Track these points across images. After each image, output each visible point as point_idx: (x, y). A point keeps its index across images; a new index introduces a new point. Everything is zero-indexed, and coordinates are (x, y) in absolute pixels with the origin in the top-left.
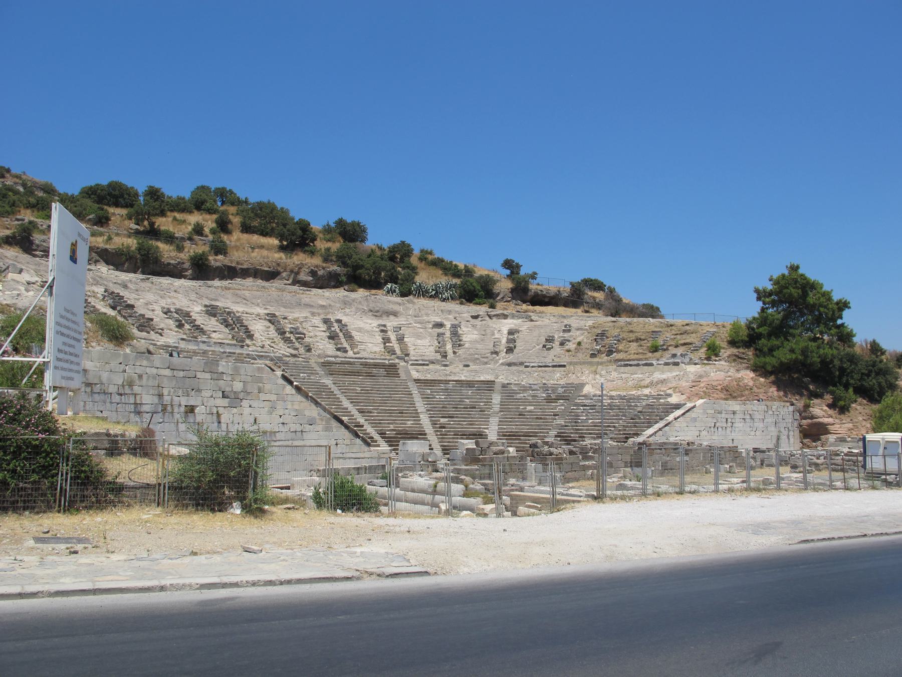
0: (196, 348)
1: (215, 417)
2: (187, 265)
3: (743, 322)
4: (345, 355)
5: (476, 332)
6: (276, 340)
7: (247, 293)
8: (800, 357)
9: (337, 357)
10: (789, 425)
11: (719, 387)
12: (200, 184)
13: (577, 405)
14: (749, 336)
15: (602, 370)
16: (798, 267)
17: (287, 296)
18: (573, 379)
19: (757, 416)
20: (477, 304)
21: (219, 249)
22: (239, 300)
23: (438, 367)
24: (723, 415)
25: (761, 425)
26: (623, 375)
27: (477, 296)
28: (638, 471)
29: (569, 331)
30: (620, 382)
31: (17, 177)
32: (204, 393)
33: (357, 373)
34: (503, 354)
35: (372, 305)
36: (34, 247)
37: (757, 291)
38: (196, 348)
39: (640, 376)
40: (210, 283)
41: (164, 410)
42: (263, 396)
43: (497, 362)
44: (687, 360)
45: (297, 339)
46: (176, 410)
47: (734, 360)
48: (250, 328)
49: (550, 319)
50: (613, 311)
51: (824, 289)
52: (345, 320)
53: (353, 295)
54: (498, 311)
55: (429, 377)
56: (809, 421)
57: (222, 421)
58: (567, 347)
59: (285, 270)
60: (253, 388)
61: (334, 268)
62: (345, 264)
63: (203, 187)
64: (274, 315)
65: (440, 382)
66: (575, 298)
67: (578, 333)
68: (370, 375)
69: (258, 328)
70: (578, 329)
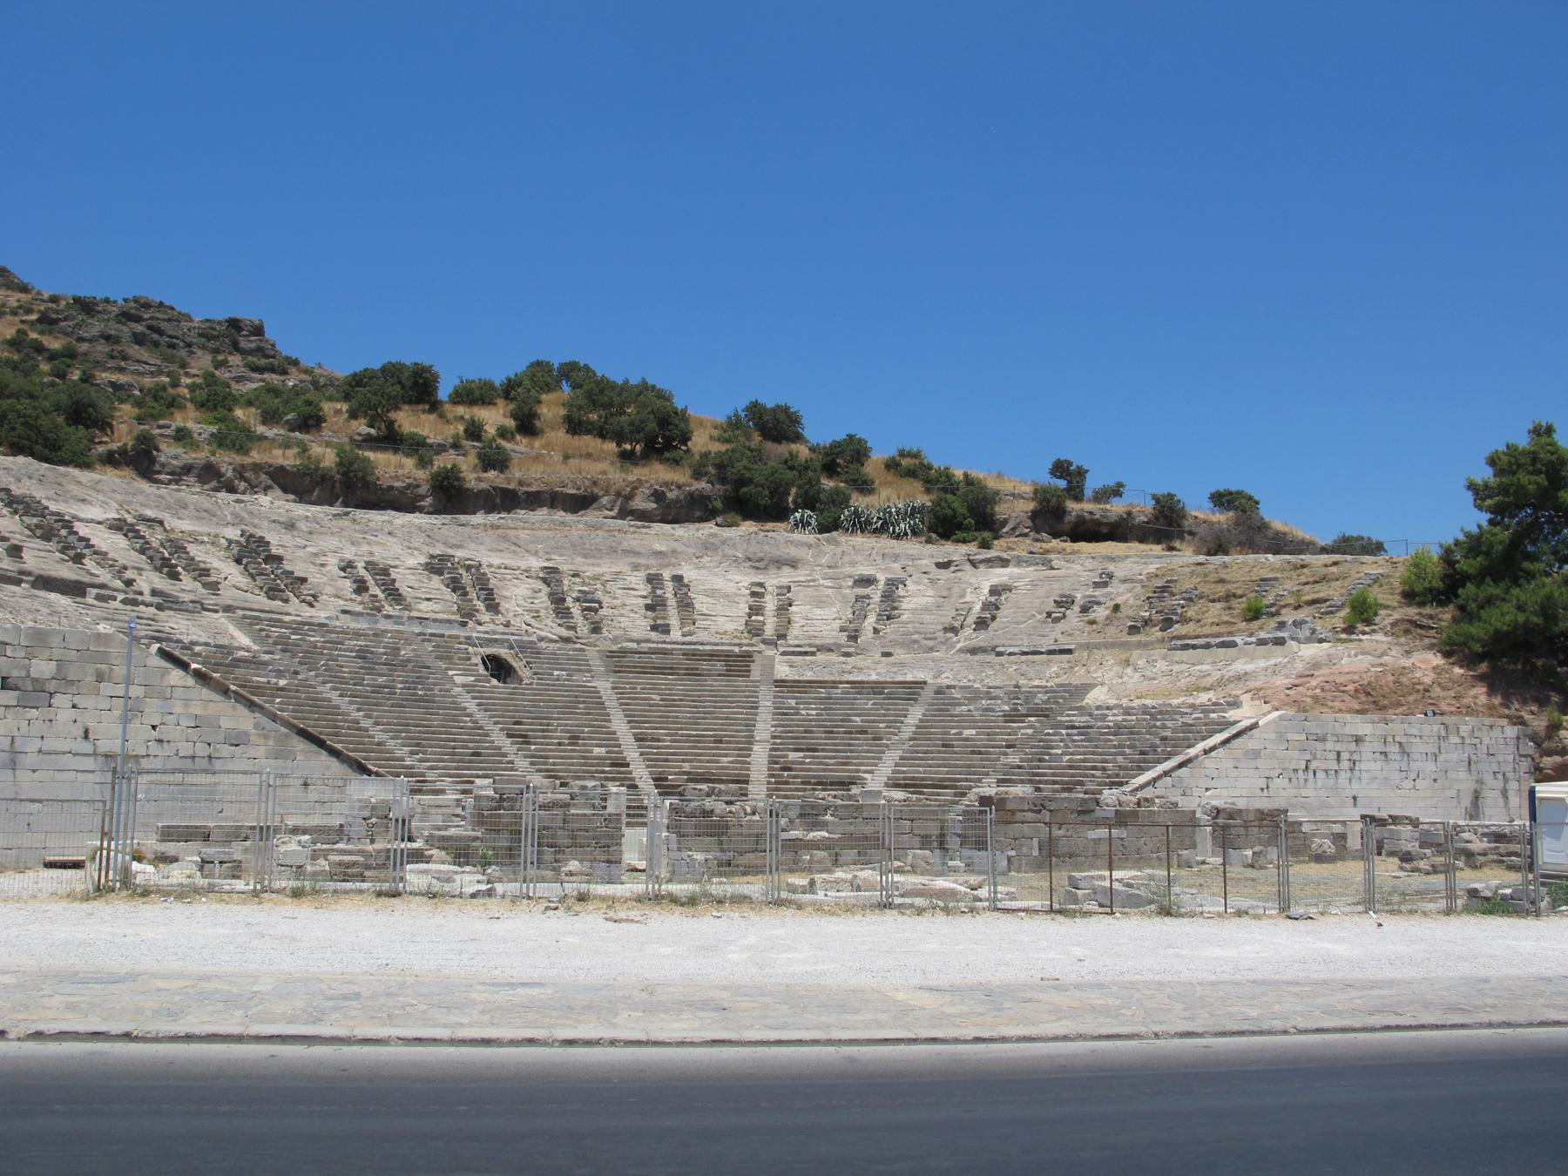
2: (423, 490)
3: (1435, 554)
5: (930, 592)
7: (523, 534)
8: (1535, 619)
10: (1508, 769)
11: (1351, 687)
12: (533, 359)
13: (1061, 725)
14: (1445, 577)
15: (1140, 657)
16: (1549, 430)
18: (1079, 676)
19: (1418, 747)
20: (958, 541)
21: (494, 460)
23: (833, 657)
24: (1329, 745)
25: (1430, 767)
26: (1176, 668)
27: (960, 527)
28: (980, 856)
29: (1105, 584)
31: (307, 371)
35: (754, 549)
36: (157, 467)
37: (1472, 486)
40: (463, 518)
42: (107, 688)
47: (1407, 632)
49: (1079, 565)
51: (497, 383)
54: (991, 554)
55: (809, 675)
56: (1558, 759)
58: (1092, 616)
59: (607, 493)
61: (702, 485)
62: (723, 480)
63: (539, 364)
64: (555, 570)
66: (1165, 524)
67: (1123, 587)
68: (693, 673)
69: (521, 600)
70: (1124, 581)
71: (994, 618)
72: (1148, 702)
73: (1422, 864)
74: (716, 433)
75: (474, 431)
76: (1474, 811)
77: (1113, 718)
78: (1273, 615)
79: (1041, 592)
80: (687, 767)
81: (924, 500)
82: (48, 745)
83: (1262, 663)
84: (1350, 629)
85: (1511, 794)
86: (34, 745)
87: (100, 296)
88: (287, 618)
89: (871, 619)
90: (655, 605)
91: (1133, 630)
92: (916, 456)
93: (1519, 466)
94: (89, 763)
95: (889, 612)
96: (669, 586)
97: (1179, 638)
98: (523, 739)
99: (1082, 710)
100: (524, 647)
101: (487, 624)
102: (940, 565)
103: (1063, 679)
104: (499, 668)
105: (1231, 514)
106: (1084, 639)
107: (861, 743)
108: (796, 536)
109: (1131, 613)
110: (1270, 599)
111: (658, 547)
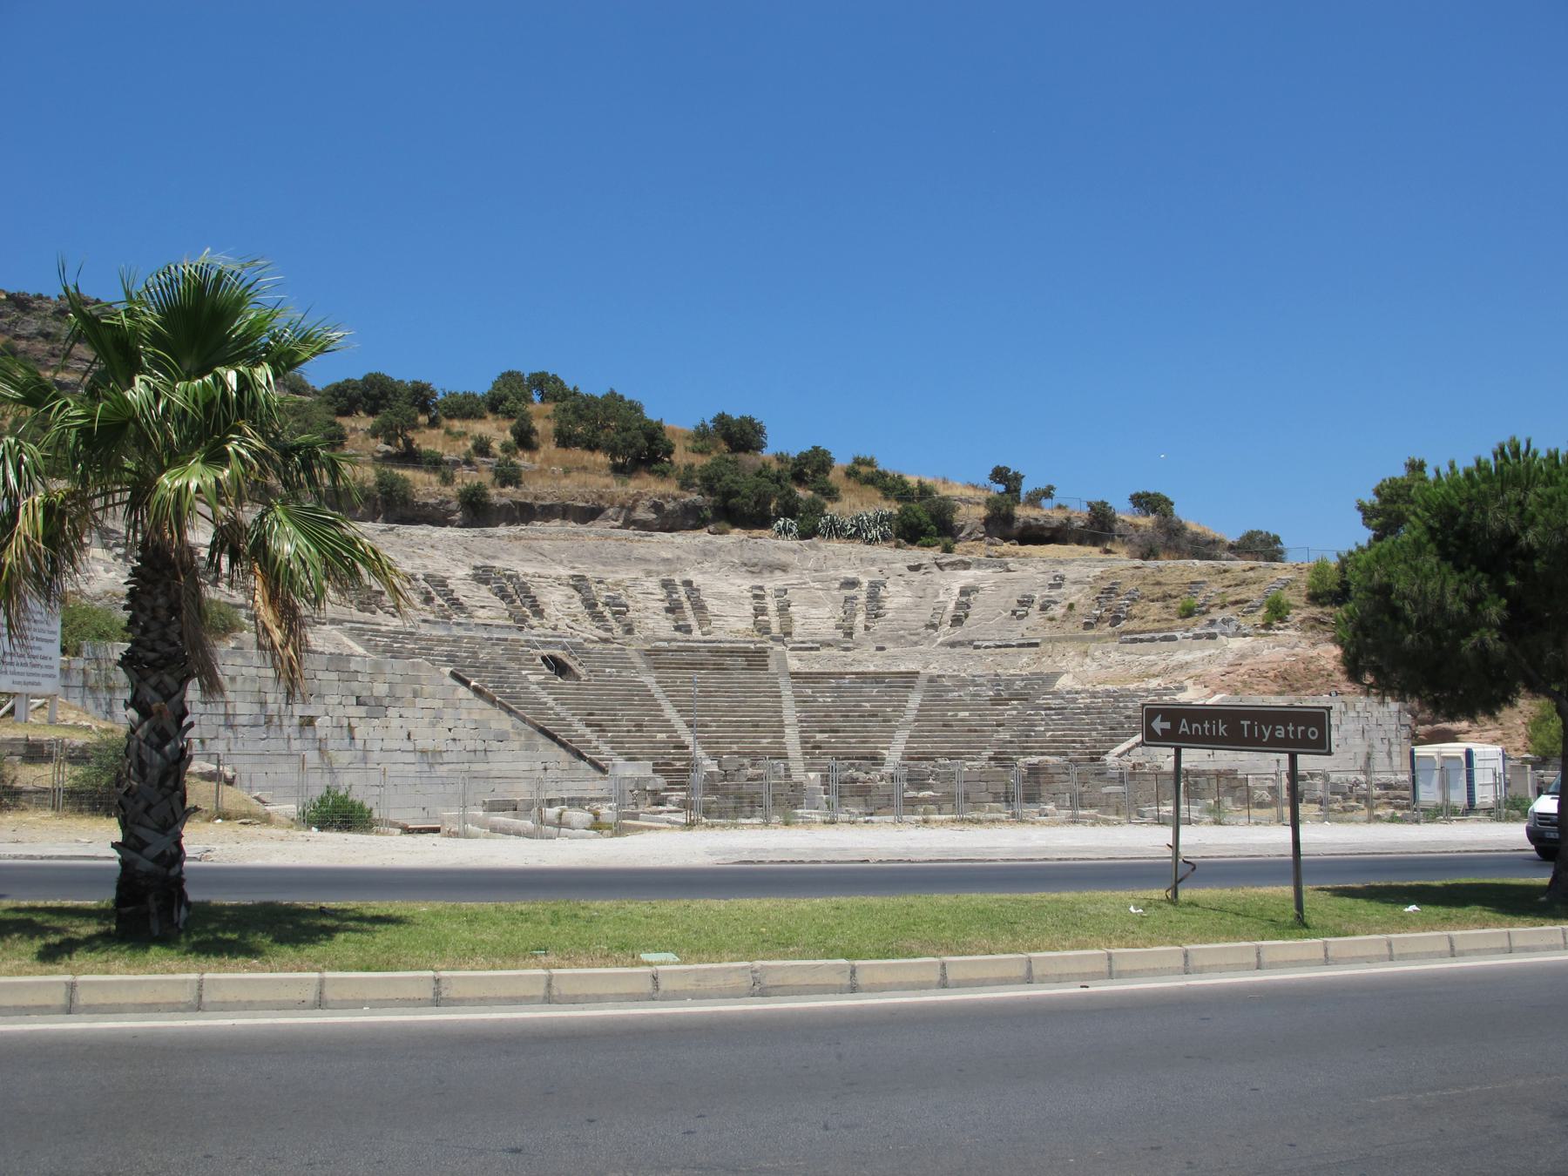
0: (443, 633)
1: (345, 732)
2: (454, 505)
3: (1333, 562)
4: (687, 636)
6: (580, 617)
7: (546, 545)
9: (675, 640)
10: (1392, 736)
11: (1271, 674)
12: (505, 370)
17: (611, 545)
18: (1046, 666)
21: (508, 476)
22: (533, 555)
23: (835, 651)
26: (1127, 658)
27: (924, 533)
29: (1059, 586)
30: (1119, 669)
32: (327, 700)
33: (699, 666)
34: (946, 628)
35: (747, 555)
37: (1361, 507)
38: (443, 633)
39: (1152, 658)
40: (489, 530)
41: (269, 721)
43: (934, 641)
44: (1231, 629)
45: (614, 614)
46: (286, 722)
47: (1312, 627)
48: (541, 599)
49: (1034, 567)
50: (1145, 550)
52: (698, 580)
53: (721, 540)
54: (954, 557)
55: (817, 668)
57: (357, 735)
58: (1050, 614)
59: (612, 505)
60: (405, 691)
61: (693, 497)
62: (711, 490)
63: (510, 374)
64: (582, 578)
65: (830, 675)
66: (1099, 529)
67: (1074, 588)
68: (720, 668)
69: (557, 601)
70: (1075, 583)
71: (967, 616)
72: (1109, 687)
73: (1336, 806)
74: (690, 444)
75: (482, 448)
76: (1366, 770)
77: (1083, 701)
78: (1204, 613)
79: (1005, 592)
80: (735, 748)
81: (891, 508)
82: (388, 744)
83: (1198, 654)
84: (1268, 626)
85: (1394, 755)
86: (377, 746)
87: (32, 292)
88: (383, 629)
89: (861, 618)
90: (673, 609)
91: (1088, 626)
92: (870, 463)
93: (1399, 496)
94: (411, 758)
95: (875, 612)
96: (682, 590)
97: (1128, 633)
98: (599, 727)
99: (1055, 694)
100: (577, 647)
101: (537, 630)
102: (911, 568)
103: (1034, 668)
104: (558, 667)
105: (1153, 517)
106: (1047, 633)
107: (874, 724)
108: (780, 542)
109: (1083, 611)
110: (1200, 600)
111: (664, 555)
